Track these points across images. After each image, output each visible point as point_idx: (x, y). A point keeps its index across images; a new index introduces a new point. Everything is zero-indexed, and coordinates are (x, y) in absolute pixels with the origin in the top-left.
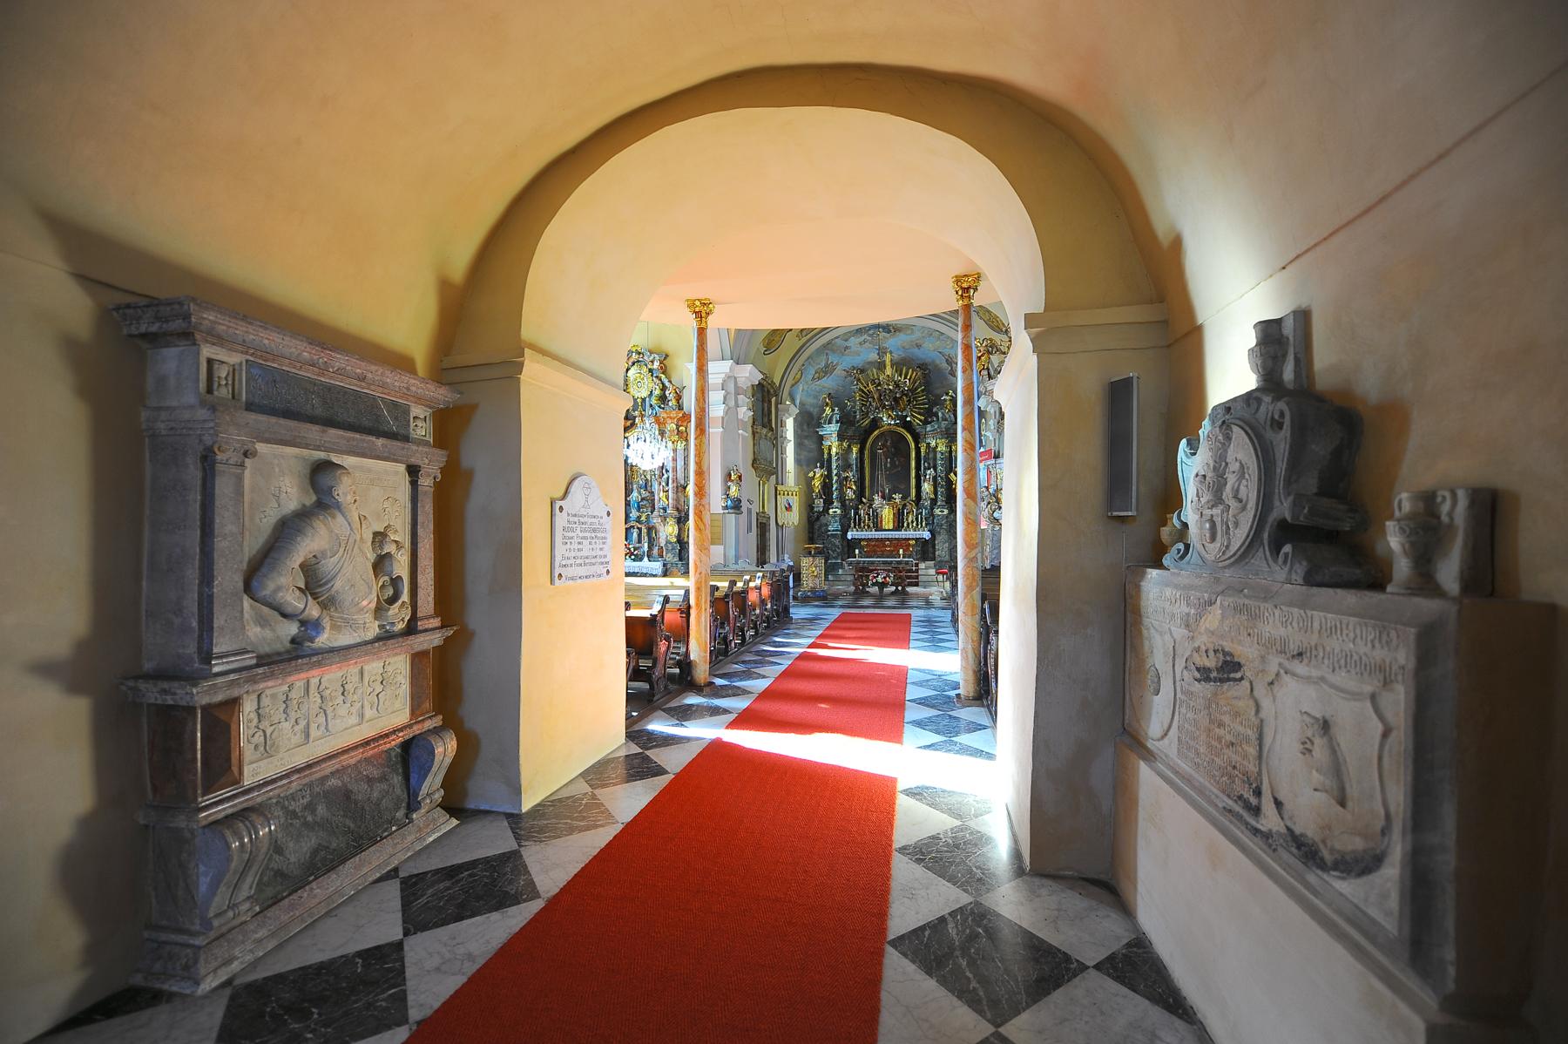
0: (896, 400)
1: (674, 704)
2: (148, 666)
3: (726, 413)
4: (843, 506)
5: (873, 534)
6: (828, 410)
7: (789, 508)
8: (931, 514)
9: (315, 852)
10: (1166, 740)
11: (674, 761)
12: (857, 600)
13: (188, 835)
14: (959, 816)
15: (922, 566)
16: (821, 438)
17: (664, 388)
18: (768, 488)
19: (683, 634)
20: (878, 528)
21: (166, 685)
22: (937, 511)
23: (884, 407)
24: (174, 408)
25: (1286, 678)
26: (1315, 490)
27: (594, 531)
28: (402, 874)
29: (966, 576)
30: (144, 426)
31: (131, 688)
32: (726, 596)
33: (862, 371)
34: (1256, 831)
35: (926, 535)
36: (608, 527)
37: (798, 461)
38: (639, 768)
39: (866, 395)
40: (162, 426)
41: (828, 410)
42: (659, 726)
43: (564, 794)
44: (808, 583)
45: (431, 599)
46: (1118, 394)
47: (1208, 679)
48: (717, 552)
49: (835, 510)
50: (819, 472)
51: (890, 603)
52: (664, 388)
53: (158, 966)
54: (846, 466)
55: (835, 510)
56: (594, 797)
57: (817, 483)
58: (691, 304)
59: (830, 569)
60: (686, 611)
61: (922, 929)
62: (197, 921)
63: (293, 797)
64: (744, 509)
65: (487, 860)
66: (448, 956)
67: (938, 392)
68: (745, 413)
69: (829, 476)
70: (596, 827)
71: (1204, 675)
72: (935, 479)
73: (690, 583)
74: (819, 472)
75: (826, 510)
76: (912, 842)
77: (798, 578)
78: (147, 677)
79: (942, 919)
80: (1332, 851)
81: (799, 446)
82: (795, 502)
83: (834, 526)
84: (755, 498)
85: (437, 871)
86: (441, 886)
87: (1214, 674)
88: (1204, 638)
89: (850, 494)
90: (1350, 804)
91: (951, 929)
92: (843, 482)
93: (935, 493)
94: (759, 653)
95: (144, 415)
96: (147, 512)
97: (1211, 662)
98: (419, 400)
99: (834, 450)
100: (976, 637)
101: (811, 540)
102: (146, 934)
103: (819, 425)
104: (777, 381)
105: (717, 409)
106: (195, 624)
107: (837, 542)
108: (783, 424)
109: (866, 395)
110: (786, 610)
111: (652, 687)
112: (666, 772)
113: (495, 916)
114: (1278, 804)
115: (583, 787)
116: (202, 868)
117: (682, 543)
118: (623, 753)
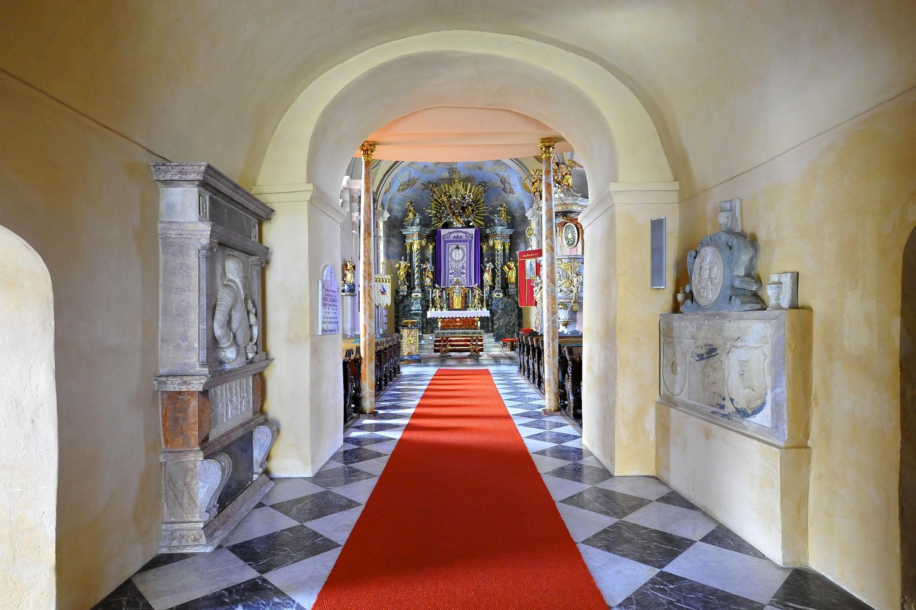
0: (463, 209)
2: (162, 371)
4: (423, 291)
5: (446, 314)
6: (411, 215)
7: (383, 292)
8: (490, 296)
10: (683, 394)
12: (443, 361)
13: (190, 466)
14: (707, 315)
16: (404, 237)
20: (450, 308)
22: (495, 295)
24: (183, 223)
33: (437, 185)
37: (387, 256)
39: (440, 205)
40: (174, 232)
41: (411, 215)
43: (327, 468)
46: (657, 226)
47: (702, 359)
49: (417, 294)
50: (403, 264)
53: (175, 543)
54: (423, 260)
55: (417, 294)
57: (402, 273)
62: (198, 515)
67: (494, 203)
69: (411, 267)
71: (701, 357)
72: (493, 271)
81: (388, 243)
83: (416, 307)
88: (700, 342)
89: (428, 281)
92: (422, 271)
93: (493, 281)
95: (160, 226)
96: (161, 282)
97: (703, 351)
99: (416, 247)
100: (556, 371)
102: (164, 527)
103: (403, 227)
106: (196, 346)
109: (440, 205)
114: (732, 400)
116: (201, 484)
118: (342, 450)
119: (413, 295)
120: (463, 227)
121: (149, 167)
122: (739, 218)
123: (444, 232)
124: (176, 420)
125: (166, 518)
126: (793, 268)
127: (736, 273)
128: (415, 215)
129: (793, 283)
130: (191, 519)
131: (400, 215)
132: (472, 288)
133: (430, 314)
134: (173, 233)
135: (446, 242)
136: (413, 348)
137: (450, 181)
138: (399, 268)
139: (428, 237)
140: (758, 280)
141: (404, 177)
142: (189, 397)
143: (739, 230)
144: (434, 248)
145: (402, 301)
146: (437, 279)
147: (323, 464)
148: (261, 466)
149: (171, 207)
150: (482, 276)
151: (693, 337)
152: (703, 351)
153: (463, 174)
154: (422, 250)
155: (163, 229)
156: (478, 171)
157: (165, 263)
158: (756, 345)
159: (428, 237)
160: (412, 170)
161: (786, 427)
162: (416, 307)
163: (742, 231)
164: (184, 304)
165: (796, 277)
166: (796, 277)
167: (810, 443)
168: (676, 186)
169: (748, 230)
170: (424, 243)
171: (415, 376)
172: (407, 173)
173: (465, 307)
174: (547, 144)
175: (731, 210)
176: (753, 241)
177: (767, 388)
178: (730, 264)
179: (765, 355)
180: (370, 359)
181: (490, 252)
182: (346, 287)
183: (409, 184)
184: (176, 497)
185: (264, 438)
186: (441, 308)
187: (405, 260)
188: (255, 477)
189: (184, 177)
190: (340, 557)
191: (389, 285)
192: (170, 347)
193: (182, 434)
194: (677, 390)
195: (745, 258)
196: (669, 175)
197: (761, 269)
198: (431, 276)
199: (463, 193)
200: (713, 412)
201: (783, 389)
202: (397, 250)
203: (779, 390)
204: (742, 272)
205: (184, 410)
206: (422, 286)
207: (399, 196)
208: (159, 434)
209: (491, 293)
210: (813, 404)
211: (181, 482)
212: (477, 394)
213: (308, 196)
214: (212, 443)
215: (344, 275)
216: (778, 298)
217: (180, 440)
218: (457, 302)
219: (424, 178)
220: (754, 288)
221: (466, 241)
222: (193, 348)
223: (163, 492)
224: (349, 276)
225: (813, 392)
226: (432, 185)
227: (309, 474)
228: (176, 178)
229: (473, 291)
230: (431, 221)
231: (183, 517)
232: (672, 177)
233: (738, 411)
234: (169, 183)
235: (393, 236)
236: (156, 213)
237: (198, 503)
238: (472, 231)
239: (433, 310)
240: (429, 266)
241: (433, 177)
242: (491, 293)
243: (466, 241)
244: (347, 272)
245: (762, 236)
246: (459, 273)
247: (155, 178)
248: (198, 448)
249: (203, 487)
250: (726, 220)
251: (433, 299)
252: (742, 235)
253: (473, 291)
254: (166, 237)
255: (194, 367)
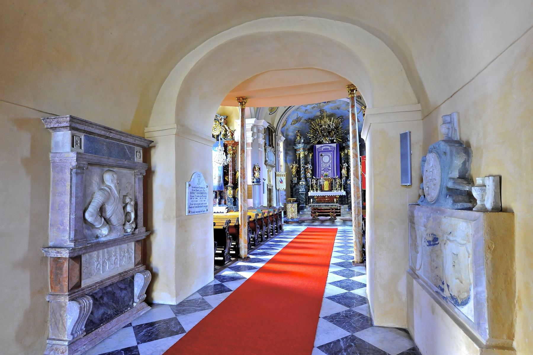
1: (233, 265)
2: (51, 244)
3: (253, 140)
4: (306, 180)
5: (319, 193)
6: (298, 138)
7: (281, 182)
9: (104, 314)
11: (233, 286)
12: (313, 222)
13: (64, 304)
15: (342, 207)
17: (226, 131)
18: (272, 174)
19: (236, 237)
20: (322, 190)
21: (59, 250)
23: (323, 136)
24: (62, 153)
25: (448, 242)
26: (458, 176)
27: (202, 193)
28: (133, 325)
29: (355, 210)
30: (50, 159)
31: (46, 251)
32: (254, 220)
34: (444, 297)
35: (344, 193)
36: (207, 192)
37: (286, 161)
38: (219, 289)
40: (57, 159)
41: (298, 138)
42: (227, 273)
43: (191, 298)
44: (290, 215)
45: (142, 220)
46: (404, 137)
48: (251, 201)
49: (303, 182)
50: (295, 165)
51: (327, 224)
52: (226, 131)
54: (306, 163)
56: (203, 299)
57: (294, 170)
58: (238, 99)
59: (300, 209)
60: (237, 227)
61: (330, 343)
62: (66, 336)
63: (96, 293)
64: (261, 183)
65: (164, 321)
66: (154, 350)
68: (262, 141)
70: (205, 309)
73: (238, 214)
74: (295, 165)
75: (298, 182)
76: (329, 315)
77: (285, 213)
78: (51, 247)
79: (338, 340)
80: (461, 299)
81: (286, 154)
82: (284, 179)
83: (302, 190)
84: (266, 178)
85: (146, 324)
86: (149, 329)
87: (432, 243)
89: (309, 175)
90: (463, 282)
91: (342, 343)
94: (268, 245)
96: (51, 189)
98: (138, 145)
99: (302, 156)
101: (292, 196)
102: (48, 341)
103: (295, 145)
104: (275, 126)
105: (249, 138)
106: (68, 229)
107: (303, 197)
108: (278, 145)
110: (281, 227)
111: (224, 258)
112: (231, 291)
113: (170, 338)
114: (448, 286)
115: (198, 296)
116: (68, 316)
117: (235, 198)
118: (213, 284)
119: (300, 183)
120: (329, 143)
121: (41, 120)
122: (457, 128)
123: (318, 146)
124: (57, 274)
125: (51, 336)
126: (496, 172)
127: (451, 176)
128: (300, 138)
129: (496, 187)
130: (63, 338)
131: (293, 138)
132: (335, 179)
133: (310, 194)
134: (57, 159)
135: (319, 152)
136: (294, 214)
137: (322, 118)
138: (292, 168)
139: (309, 150)
140: (470, 181)
141: (294, 117)
142: (64, 261)
143: (457, 138)
144: (313, 156)
145: (295, 186)
146: (314, 173)
147: (189, 295)
148: (138, 298)
149: (57, 143)
150: (341, 170)
151: (425, 226)
152: (431, 239)
153: (329, 112)
154: (306, 157)
155: (52, 157)
156: (337, 110)
157: (54, 177)
158: (463, 242)
159: (309, 150)
160: (299, 113)
161: (487, 326)
162: (302, 190)
163: (460, 139)
164: (62, 203)
165: (499, 181)
166: (499, 181)
167: (515, 344)
168: (419, 107)
169: (464, 139)
170: (306, 153)
171: (292, 232)
172: (296, 114)
173: (331, 190)
174: (352, 88)
175: (450, 123)
176: (465, 148)
177: (470, 284)
178: (445, 168)
179: (469, 254)
180: (245, 225)
181: (346, 157)
182: (255, 180)
183: (298, 120)
184: (56, 324)
185: (140, 281)
186: (317, 190)
187: (296, 163)
188: (135, 304)
189: (60, 125)
190: (320, 309)
191: (285, 178)
192: (55, 230)
193: (59, 283)
194: (418, 267)
195: (458, 162)
196: (414, 99)
197: (473, 172)
198: (311, 172)
199: (327, 123)
200: (437, 292)
201: (483, 288)
202: (291, 158)
203: (480, 289)
204: (456, 174)
205: (61, 269)
206: (306, 178)
207: (292, 128)
208: (47, 283)
209: (346, 181)
210: (517, 306)
211: (58, 314)
212: (322, 246)
213: (174, 131)
214: (83, 289)
215: (254, 174)
216: (483, 200)
217: (58, 288)
218: (326, 188)
219: (307, 116)
220: (467, 188)
221: (331, 151)
222: (67, 230)
223: (49, 319)
224: (257, 174)
225: (517, 294)
226: (310, 120)
227: (174, 303)
228: (56, 126)
229: (335, 180)
230: (310, 141)
231: (59, 337)
232: (416, 101)
233: (452, 297)
234: (54, 129)
235: (289, 150)
236: (48, 149)
237: (67, 328)
238: (334, 145)
239: (312, 191)
240: (309, 166)
241: (311, 116)
242: (346, 181)
243: (331, 151)
244: (255, 172)
245: (474, 143)
246: (326, 170)
247: (46, 127)
248: (67, 293)
249: (70, 319)
250: (447, 131)
251: (312, 185)
252: (459, 143)
253: (335, 180)
254: (54, 162)
255: (67, 241)
